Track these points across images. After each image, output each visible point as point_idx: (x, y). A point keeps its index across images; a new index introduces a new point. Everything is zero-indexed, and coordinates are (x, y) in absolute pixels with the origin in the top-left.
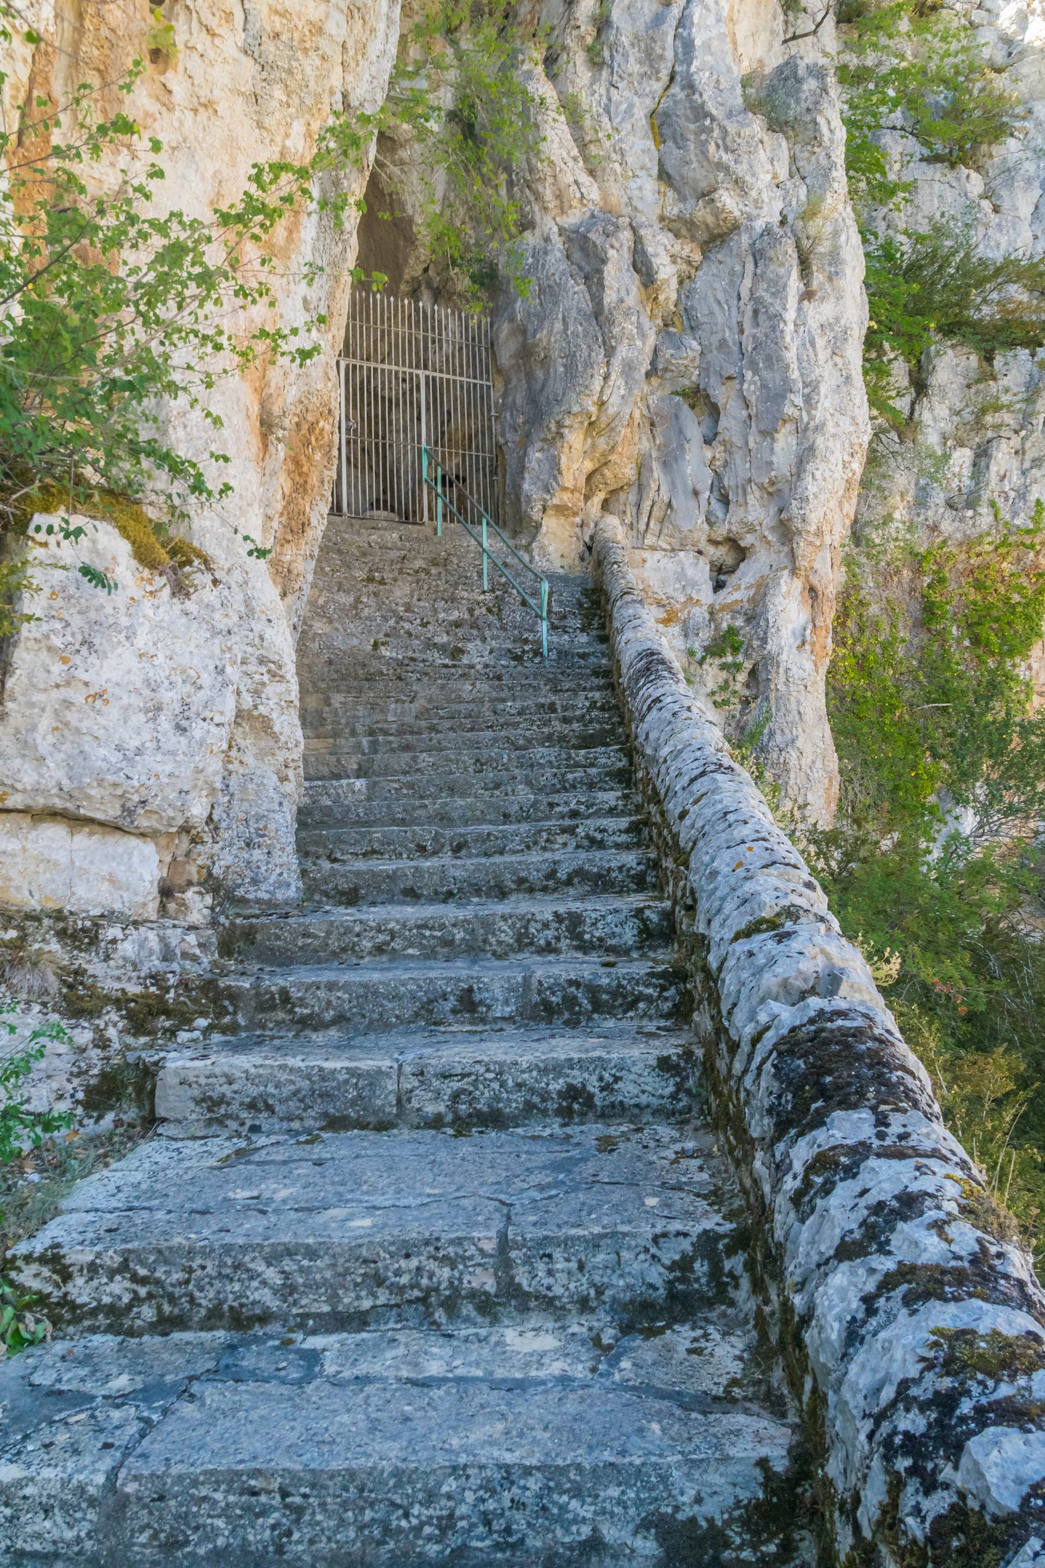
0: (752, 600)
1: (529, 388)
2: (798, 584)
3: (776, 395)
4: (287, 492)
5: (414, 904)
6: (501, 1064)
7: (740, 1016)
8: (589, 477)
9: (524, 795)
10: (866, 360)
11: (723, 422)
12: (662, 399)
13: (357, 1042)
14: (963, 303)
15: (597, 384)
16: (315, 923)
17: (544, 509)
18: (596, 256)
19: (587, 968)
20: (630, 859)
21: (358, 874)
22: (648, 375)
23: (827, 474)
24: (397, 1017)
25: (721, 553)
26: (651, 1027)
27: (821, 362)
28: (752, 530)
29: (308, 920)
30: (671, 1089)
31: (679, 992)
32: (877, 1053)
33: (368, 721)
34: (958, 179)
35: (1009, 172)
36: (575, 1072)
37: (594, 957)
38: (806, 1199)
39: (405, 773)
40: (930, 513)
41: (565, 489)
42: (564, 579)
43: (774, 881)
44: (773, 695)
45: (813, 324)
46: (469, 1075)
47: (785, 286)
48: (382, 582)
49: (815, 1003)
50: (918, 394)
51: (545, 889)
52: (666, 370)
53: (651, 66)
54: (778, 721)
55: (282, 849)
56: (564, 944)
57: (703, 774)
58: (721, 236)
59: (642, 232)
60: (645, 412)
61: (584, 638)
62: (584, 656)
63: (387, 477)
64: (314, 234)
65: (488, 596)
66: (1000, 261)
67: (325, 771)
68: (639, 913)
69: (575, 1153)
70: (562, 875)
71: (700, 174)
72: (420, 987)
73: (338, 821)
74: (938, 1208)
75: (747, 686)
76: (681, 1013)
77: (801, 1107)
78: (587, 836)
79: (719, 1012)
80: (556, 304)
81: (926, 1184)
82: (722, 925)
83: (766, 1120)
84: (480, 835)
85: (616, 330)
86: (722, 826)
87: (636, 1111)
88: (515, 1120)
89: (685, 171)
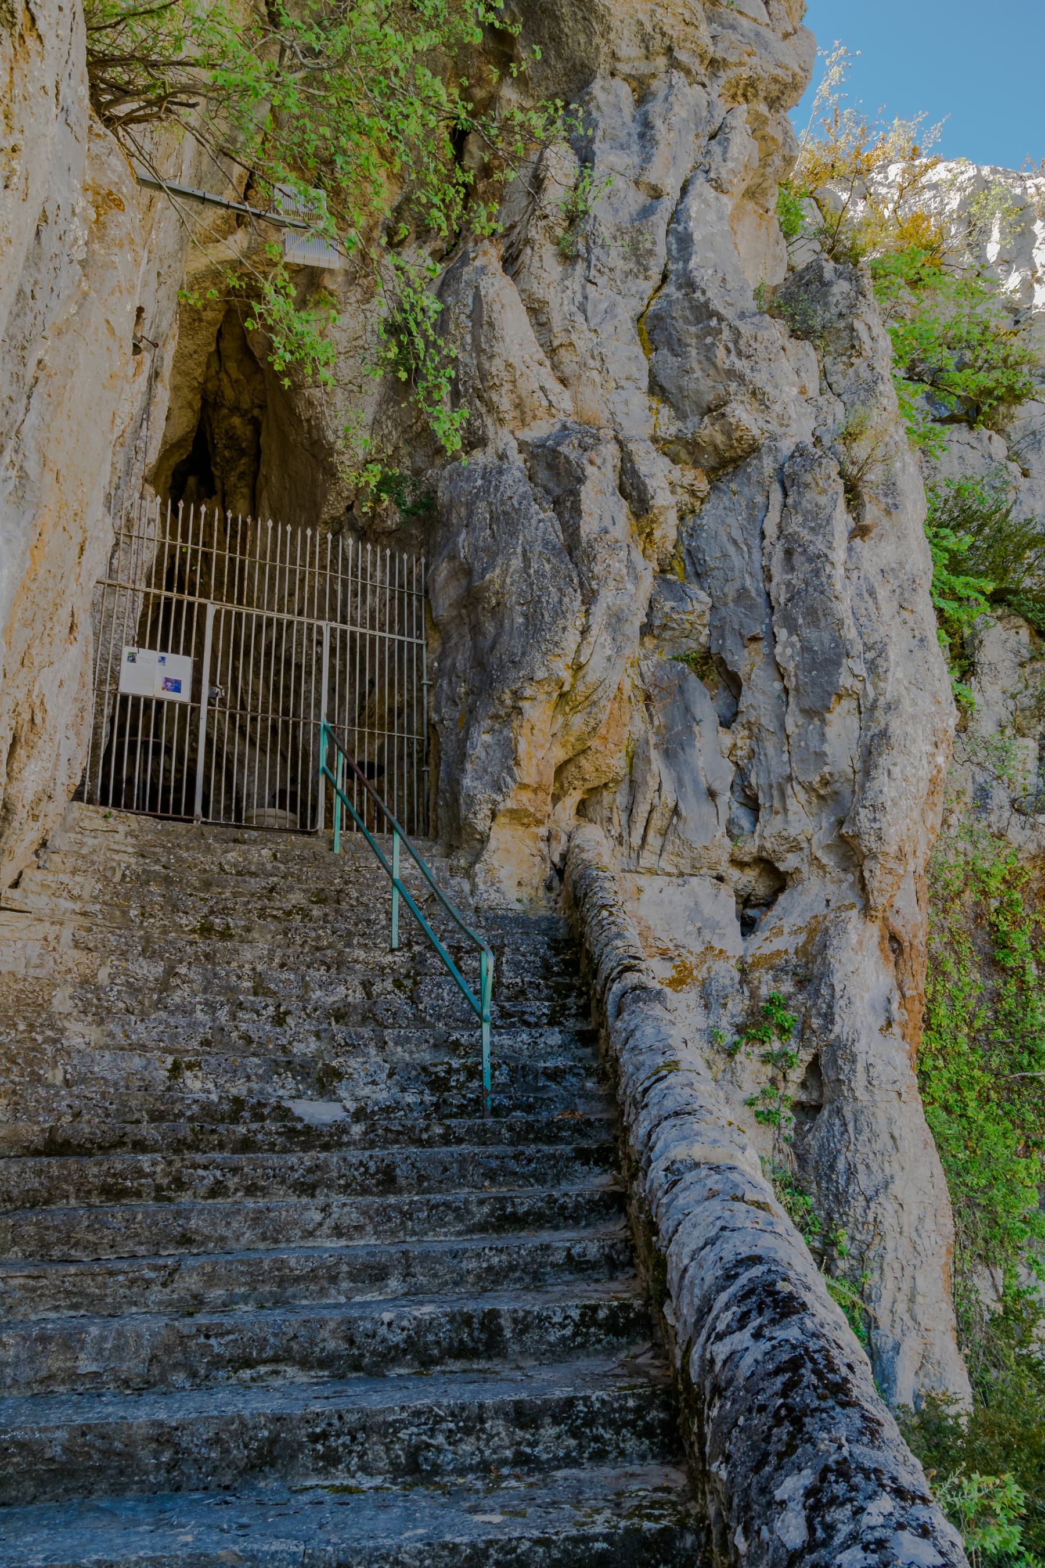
1: (475, 646)
2: (873, 931)
3: (824, 662)
8: (560, 770)
11: (746, 699)
12: (659, 665)
15: (571, 639)
17: (494, 816)
18: (570, 473)
23: (910, 771)
25: (750, 879)
27: (886, 618)
34: (980, 440)
40: (993, 818)
41: (524, 786)
42: (521, 921)
45: (870, 568)
52: (665, 627)
53: (638, 263)
54: (858, 1151)
58: (733, 460)
59: (631, 446)
60: (638, 682)
75: (803, 1085)
80: (513, 534)
85: (598, 569)
89: (685, 381)
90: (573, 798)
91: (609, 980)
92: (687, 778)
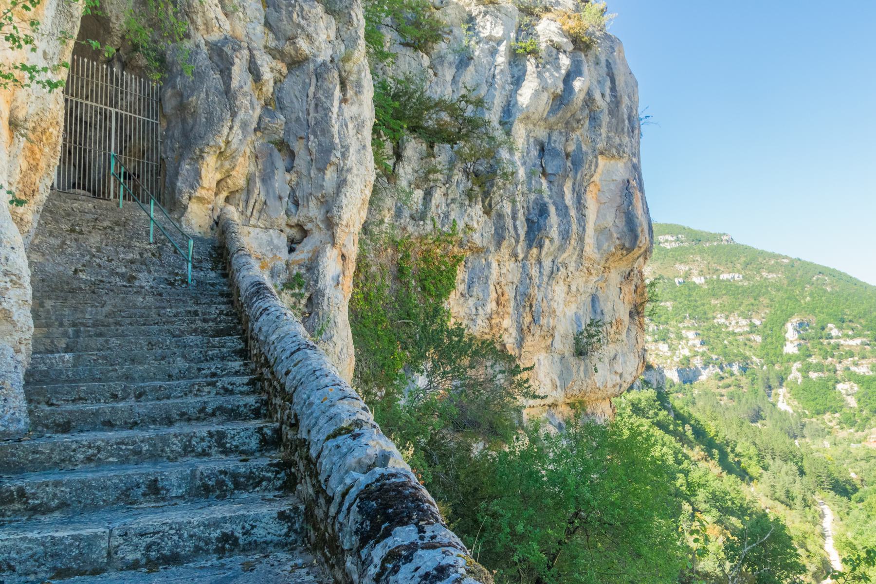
0: (310, 259)
1: (183, 128)
3: (326, 150)
4: (24, 169)
5: (111, 431)
6: (180, 524)
7: (333, 482)
8: (219, 182)
9: (181, 363)
10: (373, 139)
11: (297, 161)
12: (262, 144)
13: (76, 518)
14: (420, 117)
15: (225, 131)
16: (43, 446)
17: (190, 198)
18: (227, 60)
19: (231, 463)
20: (251, 400)
21: (71, 412)
22: (255, 130)
24: (104, 501)
25: (294, 233)
26: (270, 496)
28: (311, 221)
29: (37, 442)
30: (286, 530)
31: (287, 475)
32: (415, 494)
33: (71, 318)
34: (418, 57)
35: (441, 58)
36: (228, 525)
37: (232, 457)
38: (383, 577)
39: (99, 350)
40: (402, 221)
43: (347, 407)
44: (321, 314)
46: (158, 533)
47: (333, 94)
48: (81, 233)
49: (378, 470)
50: (397, 160)
51: (198, 419)
52: (265, 129)
55: (16, 397)
56: (214, 450)
57: (299, 350)
59: (255, 52)
60: (253, 150)
61: (213, 274)
62: (213, 285)
63: (84, 169)
64: (53, 14)
65: (153, 246)
66: (437, 99)
67: (42, 348)
68: (260, 430)
69: (229, 573)
70: (209, 410)
71: (288, 27)
72: (121, 481)
73: (53, 380)
74: (456, 572)
75: (306, 306)
76: (289, 486)
77: (376, 528)
78: (223, 388)
79: (319, 481)
80: (202, 83)
81: (449, 560)
82: (318, 432)
83: (354, 538)
84: (155, 387)
85: (238, 103)
86: (313, 378)
87: (265, 545)
88: (188, 559)
89: (280, 24)
90: (224, 194)
91: (234, 253)
92: (270, 191)
